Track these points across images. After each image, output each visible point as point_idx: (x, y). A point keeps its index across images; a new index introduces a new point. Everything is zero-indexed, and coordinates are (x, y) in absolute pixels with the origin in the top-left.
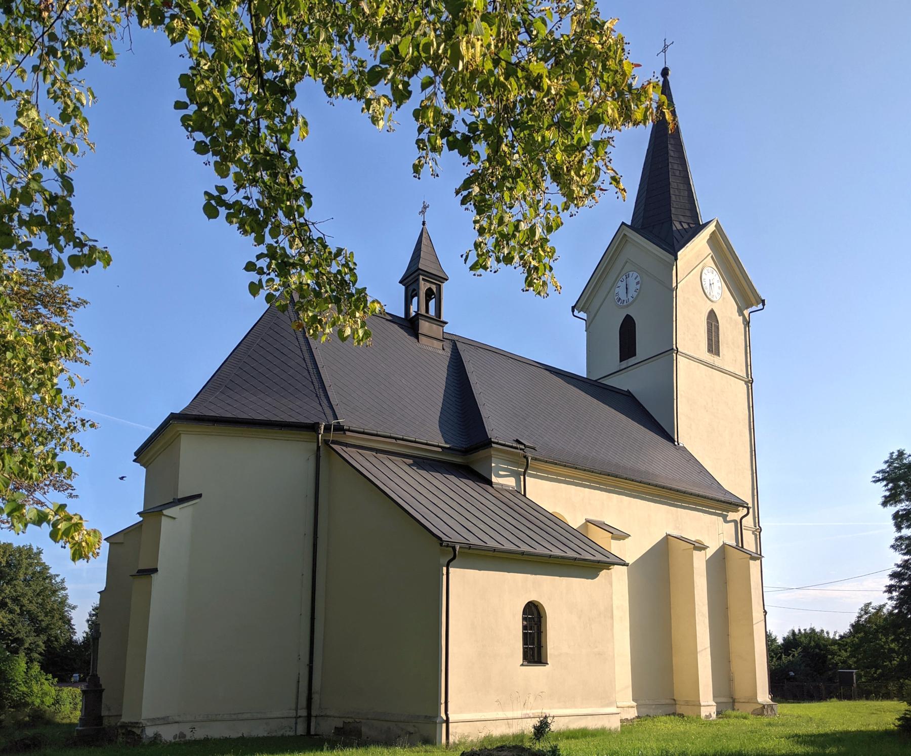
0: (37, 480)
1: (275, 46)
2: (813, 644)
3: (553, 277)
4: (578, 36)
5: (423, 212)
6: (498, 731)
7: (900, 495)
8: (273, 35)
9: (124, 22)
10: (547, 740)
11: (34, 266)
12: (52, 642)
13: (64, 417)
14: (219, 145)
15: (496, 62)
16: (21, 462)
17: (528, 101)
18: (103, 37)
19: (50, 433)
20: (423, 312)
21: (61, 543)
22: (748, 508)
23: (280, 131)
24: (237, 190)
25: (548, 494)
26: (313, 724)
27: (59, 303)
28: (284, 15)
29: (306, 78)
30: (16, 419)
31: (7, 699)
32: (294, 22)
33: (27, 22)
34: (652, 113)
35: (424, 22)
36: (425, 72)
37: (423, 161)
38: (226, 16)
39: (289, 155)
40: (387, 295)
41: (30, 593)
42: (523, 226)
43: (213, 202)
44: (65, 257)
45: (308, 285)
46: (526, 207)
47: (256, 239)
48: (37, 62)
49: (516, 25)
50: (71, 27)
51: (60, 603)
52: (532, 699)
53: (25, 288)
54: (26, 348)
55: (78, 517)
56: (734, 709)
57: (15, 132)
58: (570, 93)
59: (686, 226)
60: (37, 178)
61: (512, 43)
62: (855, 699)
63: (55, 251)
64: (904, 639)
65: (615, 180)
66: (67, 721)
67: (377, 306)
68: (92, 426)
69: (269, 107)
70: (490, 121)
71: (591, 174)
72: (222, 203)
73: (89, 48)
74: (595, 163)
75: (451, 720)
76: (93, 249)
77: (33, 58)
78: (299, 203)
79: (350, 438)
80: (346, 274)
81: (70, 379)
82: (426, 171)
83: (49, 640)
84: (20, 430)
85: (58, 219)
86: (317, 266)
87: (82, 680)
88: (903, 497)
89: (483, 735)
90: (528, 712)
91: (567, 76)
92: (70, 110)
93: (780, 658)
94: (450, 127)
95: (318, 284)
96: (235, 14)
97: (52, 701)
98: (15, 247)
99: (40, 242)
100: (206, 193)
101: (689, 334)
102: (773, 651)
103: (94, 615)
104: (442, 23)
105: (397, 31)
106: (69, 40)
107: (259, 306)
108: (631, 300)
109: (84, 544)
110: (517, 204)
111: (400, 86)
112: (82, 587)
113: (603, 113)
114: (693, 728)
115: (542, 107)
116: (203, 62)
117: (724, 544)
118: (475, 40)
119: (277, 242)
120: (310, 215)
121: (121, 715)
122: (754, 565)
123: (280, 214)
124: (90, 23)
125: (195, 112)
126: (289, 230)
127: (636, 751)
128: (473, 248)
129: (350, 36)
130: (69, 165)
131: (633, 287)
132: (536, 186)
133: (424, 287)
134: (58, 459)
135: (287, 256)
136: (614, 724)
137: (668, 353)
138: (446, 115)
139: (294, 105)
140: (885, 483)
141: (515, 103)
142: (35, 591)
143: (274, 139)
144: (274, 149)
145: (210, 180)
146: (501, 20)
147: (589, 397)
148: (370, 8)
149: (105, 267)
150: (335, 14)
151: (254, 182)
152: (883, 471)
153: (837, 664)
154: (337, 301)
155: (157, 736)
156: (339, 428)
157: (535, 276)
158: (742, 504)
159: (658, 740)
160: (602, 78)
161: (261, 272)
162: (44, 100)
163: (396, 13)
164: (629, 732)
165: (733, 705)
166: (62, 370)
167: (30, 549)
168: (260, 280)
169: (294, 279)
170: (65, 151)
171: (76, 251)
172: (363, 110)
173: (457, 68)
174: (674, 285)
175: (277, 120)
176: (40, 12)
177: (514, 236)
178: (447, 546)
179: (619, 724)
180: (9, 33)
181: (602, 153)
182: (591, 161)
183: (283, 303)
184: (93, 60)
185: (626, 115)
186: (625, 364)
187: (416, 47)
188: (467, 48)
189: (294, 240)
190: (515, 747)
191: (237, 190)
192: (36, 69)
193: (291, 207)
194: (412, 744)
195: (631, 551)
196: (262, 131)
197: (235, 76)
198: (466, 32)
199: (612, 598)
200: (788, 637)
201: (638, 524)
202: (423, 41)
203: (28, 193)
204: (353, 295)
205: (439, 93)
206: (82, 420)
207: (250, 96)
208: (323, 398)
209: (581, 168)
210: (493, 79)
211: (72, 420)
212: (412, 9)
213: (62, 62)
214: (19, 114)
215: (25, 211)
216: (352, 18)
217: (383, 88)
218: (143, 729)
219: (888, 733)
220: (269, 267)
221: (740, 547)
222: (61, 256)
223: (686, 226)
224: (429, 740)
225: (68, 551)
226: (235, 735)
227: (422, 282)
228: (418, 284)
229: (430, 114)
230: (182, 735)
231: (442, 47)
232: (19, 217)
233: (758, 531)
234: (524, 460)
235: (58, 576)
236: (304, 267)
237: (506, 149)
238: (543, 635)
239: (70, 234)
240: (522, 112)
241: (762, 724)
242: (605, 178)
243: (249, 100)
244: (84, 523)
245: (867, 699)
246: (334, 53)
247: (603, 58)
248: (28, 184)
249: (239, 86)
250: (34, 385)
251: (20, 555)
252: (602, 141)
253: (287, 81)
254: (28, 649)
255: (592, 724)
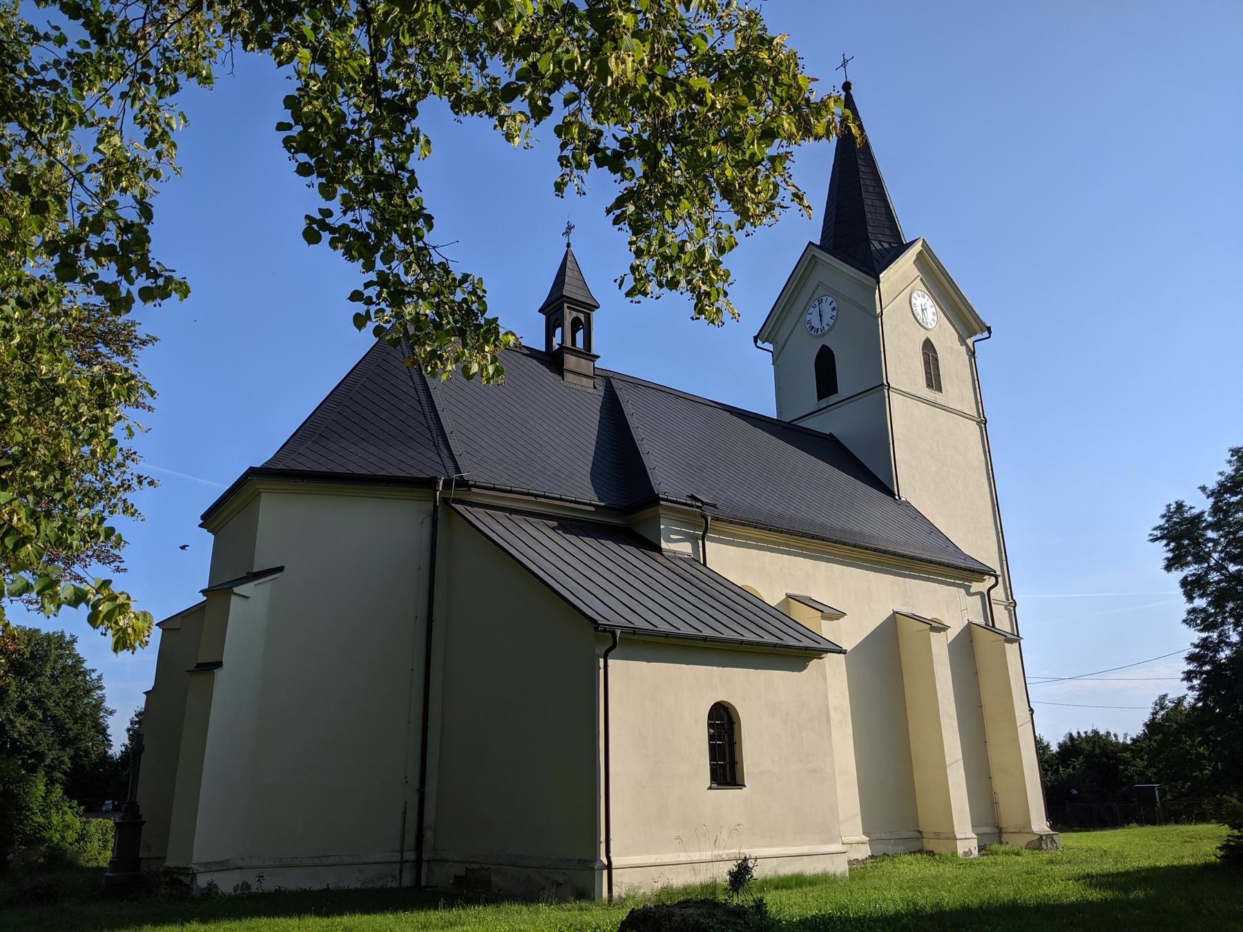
0: (77, 550)
1: (396, 65)
2: (1097, 751)
3: (728, 303)
4: (744, 52)
5: (567, 233)
6: (681, 879)
7: (1186, 556)
8: (393, 55)
9: (227, 46)
10: (749, 891)
11: (98, 300)
12: (80, 757)
13: (117, 473)
14: (327, 165)
15: (651, 77)
16: (60, 528)
17: (690, 116)
18: (202, 62)
19: (98, 493)
20: (568, 344)
21: (102, 629)
22: (996, 577)
23: (398, 150)
24: (345, 213)
25: (731, 561)
26: (424, 872)
27: (123, 341)
28: (407, 36)
29: (430, 97)
30: (58, 477)
31: (18, 833)
32: (418, 41)
33: (121, 50)
34: (835, 127)
35: (567, 39)
36: (569, 88)
37: (567, 178)
38: (342, 38)
39: (407, 175)
40: (529, 330)
41: (57, 694)
42: (689, 247)
43: (315, 226)
44: (135, 290)
45: (427, 315)
46: (692, 226)
47: (364, 266)
48: (127, 89)
49: (672, 41)
50: (168, 54)
51: (94, 706)
52: (725, 835)
53: (85, 325)
54: (78, 393)
55: (125, 596)
56: (1001, 843)
57: (93, 158)
58: (739, 108)
59: (886, 246)
60: (112, 205)
61: (669, 59)
62: (1161, 824)
63: (124, 283)
64: (1215, 741)
65: (798, 197)
66: (93, 864)
67: (512, 339)
68: (151, 483)
69: (386, 126)
70: (645, 136)
71: (768, 190)
72: (324, 226)
73: (185, 74)
74: (772, 179)
75: (614, 864)
76: (169, 280)
77: (123, 85)
78: (418, 225)
79: (476, 495)
80: (473, 302)
81: (128, 428)
82: (570, 189)
83: (76, 754)
84: (62, 490)
85: (132, 249)
86: (438, 294)
87: (116, 809)
88: (1190, 558)
89: (659, 885)
90: (721, 852)
91: (734, 91)
92: (157, 135)
93: (1057, 771)
94: (598, 142)
95: (438, 314)
96: (352, 36)
97: (75, 836)
98: (78, 280)
99: (109, 273)
100: (307, 217)
101: (902, 367)
102: (1046, 762)
103: (136, 722)
104: (587, 40)
105: (536, 48)
106: (164, 66)
107: (366, 340)
108: (827, 328)
109: (130, 630)
110: (681, 223)
111: (540, 103)
112: (123, 686)
113: (778, 128)
114: (948, 870)
115: (706, 121)
116: (312, 83)
117: (970, 623)
118: (626, 56)
119: (390, 268)
120: (429, 238)
121: (165, 858)
122: (1011, 649)
123: (395, 237)
124: (190, 49)
125: (299, 133)
126: (405, 254)
127: (873, 905)
128: (629, 271)
129: (481, 54)
130: (150, 191)
131: (828, 313)
132: (704, 204)
133: (569, 316)
134: (106, 524)
135: (402, 284)
136: (839, 867)
137: (878, 389)
138: (593, 131)
139: (415, 123)
140: (1165, 542)
141: (674, 118)
142: (63, 690)
143: (391, 159)
144: (390, 169)
145: (314, 202)
146: (654, 37)
147: (782, 443)
148: (505, 27)
149: (181, 300)
150: (464, 33)
151: (365, 204)
152: (1160, 528)
153: (1132, 777)
154: (462, 333)
155: (212, 886)
156: (463, 484)
157: (706, 302)
158: (990, 572)
159: (901, 888)
160: (774, 92)
161: (369, 301)
162: (129, 124)
163: (534, 31)
164: (861, 878)
165: (1000, 838)
166: (120, 418)
167: (62, 636)
168: (368, 312)
169: (409, 310)
170: (147, 176)
171: (149, 283)
172: (495, 127)
173: (605, 82)
174: (878, 311)
175: (395, 139)
176: (136, 41)
177: (679, 258)
178: (605, 630)
179: (847, 867)
180: (99, 62)
181: (779, 168)
182: (767, 177)
183: (395, 336)
184: (188, 85)
185: (806, 130)
186: (824, 403)
187: (558, 63)
188: (617, 64)
189: (411, 266)
190: (705, 902)
191: (345, 213)
192: (124, 96)
193: (408, 229)
194: (562, 900)
195: (848, 634)
196: (376, 150)
197: (348, 96)
198: (615, 49)
199: (827, 696)
200: (1065, 743)
201: (856, 600)
202: (566, 57)
203: (100, 221)
204: (481, 326)
205: (584, 109)
206: (139, 477)
207: (364, 115)
208: (442, 446)
209: (756, 185)
210: (647, 94)
211: (127, 476)
212: (553, 27)
213: (153, 88)
214: (100, 141)
215: (94, 241)
216: (485, 37)
217: (520, 105)
218: (193, 877)
219: (1207, 868)
220: (379, 296)
221: (990, 626)
222: (132, 288)
223: (886, 246)
224: (585, 894)
225: (110, 639)
226: (317, 886)
227: (567, 311)
228: (563, 313)
229: (575, 130)
230: (246, 886)
231: (588, 63)
232: (87, 247)
233: (1011, 605)
234: (703, 520)
235: (94, 671)
236: (422, 295)
237: (666, 165)
238: (737, 746)
239: (144, 265)
240: (683, 127)
241: (1041, 862)
242: (785, 194)
243: (362, 120)
244: (132, 604)
245: (1177, 822)
246: (463, 71)
247: (775, 72)
248: (101, 212)
249: (350, 106)
250: (85, 435)
251: (49, 645)
252: (779, 156)
253: (408, 99)
254: (49, 766)
255: (809, 868)
